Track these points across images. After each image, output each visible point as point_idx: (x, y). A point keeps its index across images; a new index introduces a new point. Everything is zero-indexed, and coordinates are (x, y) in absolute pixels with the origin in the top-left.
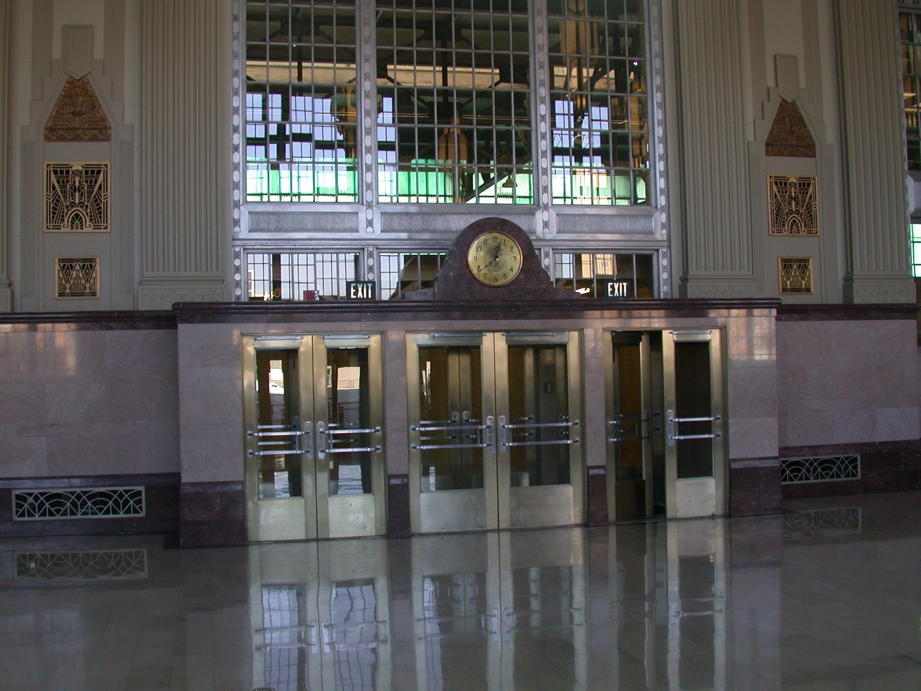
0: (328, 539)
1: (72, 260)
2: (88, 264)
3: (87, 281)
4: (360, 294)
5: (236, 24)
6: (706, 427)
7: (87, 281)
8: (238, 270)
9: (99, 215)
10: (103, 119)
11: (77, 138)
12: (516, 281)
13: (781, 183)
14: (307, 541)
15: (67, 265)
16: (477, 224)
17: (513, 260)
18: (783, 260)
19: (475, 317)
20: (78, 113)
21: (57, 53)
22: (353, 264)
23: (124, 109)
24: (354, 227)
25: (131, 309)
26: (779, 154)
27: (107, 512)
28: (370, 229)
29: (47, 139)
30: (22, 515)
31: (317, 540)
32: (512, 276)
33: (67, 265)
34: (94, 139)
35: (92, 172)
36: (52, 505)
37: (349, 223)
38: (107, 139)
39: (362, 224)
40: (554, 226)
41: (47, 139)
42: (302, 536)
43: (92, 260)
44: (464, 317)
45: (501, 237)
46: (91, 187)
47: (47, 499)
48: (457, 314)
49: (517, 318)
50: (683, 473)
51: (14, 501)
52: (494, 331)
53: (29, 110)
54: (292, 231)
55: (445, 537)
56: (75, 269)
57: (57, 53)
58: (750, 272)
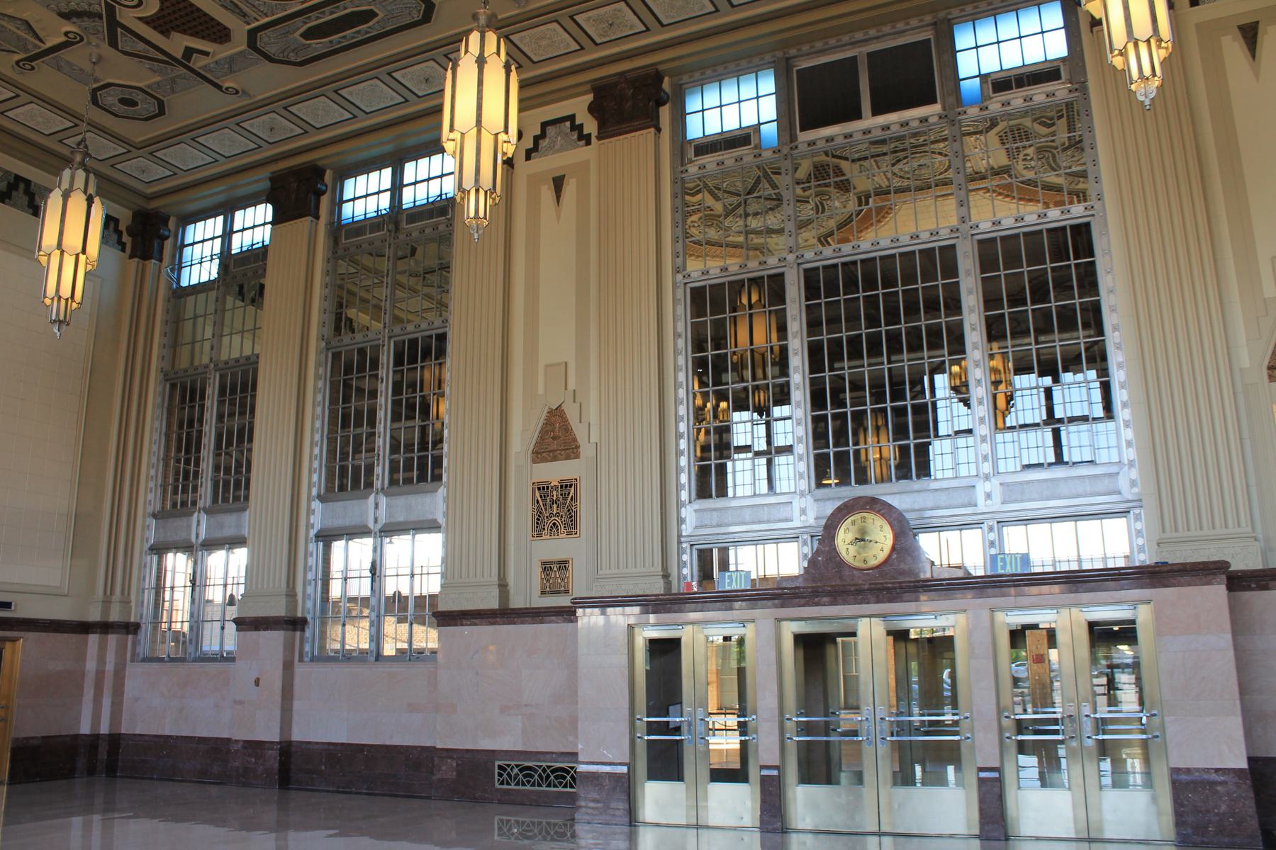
0: (708, 827)
1: (550, 563)
2: (563, 565)
3: (563, 580)
4: (1008, 567)
5: (1111, 285)
6: (651, 728)
7: (563, 580)
8: (1139, 533)
9: (571, 522)
10: (575, 440)
11: (555, 459)
12: (887, 561)
13: (543, 488)
14: (688, 826)
15: (547, 566)
16: (839, 509)
17: (883, 538)
18: (544, 563)
19: (845, 603)
20: (556, 439)
21: (541, 390)
22: (153, 592)
23: (588, 431)
24: (789, 516)
25: (1260, 567)
26: (545, 460)
27: (565, 786)
28: (803, 518)
29: (534, 461)
30: (502, 783)
31: (698, 827)
32: (882, 556)
33: (547, 566)
34: (568, 458)
35: (566, 485)
36: (525, 776)
37: (784, 512)
38: (577, 456)
39: (796, 513)
40: (997, 497)
41: (534, 461)
42: (684, 822)
43: (566, 562)
44: (834, 603)
45: (857, 517)
46: (565, 499)
47: (553, 772)
48: (825, 599)
49: (890, 601)
50: (654, 775)
51: (497, 770)
52: (870, 616)
53: (522, 439)
54: (732, 525)
55: (822, 836)
56: (555, 570)
57: (541, 390)
58: (1249, 529)
